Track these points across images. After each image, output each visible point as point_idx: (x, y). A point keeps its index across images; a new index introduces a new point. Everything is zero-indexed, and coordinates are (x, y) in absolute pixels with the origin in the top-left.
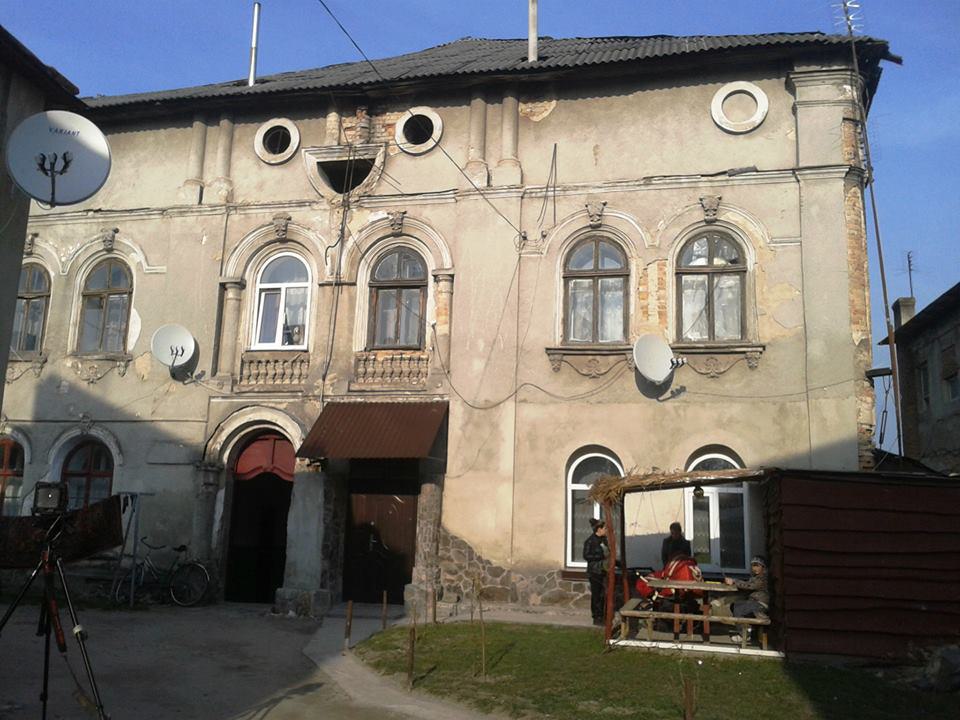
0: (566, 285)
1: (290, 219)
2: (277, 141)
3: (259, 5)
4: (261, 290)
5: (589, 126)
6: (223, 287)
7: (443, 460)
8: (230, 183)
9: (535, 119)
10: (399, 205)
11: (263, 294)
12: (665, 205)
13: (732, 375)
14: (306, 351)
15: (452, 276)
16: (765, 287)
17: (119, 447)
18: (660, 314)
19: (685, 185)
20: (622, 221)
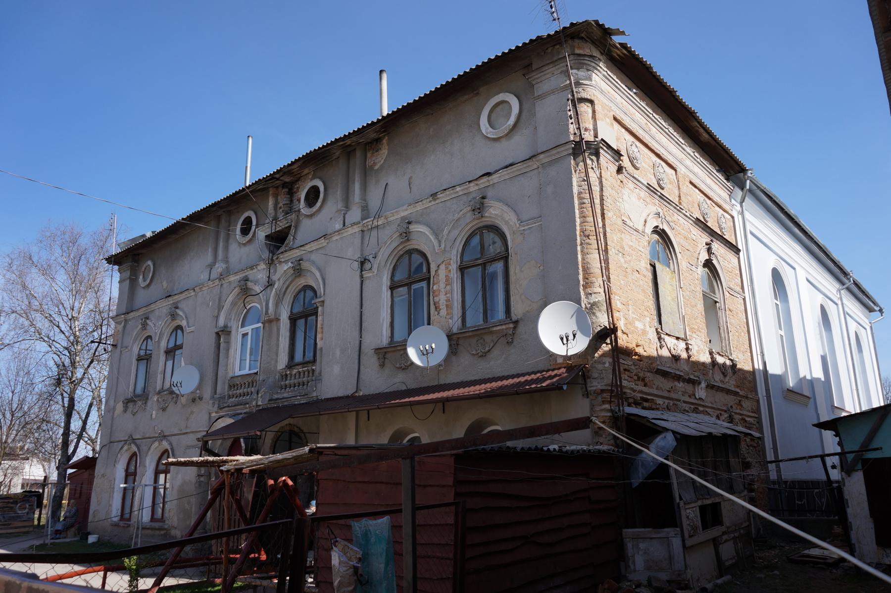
6: (217, 333)
13: (496, 352)
14: (256, 373)
18: (447, 306)
19: (461, 193)
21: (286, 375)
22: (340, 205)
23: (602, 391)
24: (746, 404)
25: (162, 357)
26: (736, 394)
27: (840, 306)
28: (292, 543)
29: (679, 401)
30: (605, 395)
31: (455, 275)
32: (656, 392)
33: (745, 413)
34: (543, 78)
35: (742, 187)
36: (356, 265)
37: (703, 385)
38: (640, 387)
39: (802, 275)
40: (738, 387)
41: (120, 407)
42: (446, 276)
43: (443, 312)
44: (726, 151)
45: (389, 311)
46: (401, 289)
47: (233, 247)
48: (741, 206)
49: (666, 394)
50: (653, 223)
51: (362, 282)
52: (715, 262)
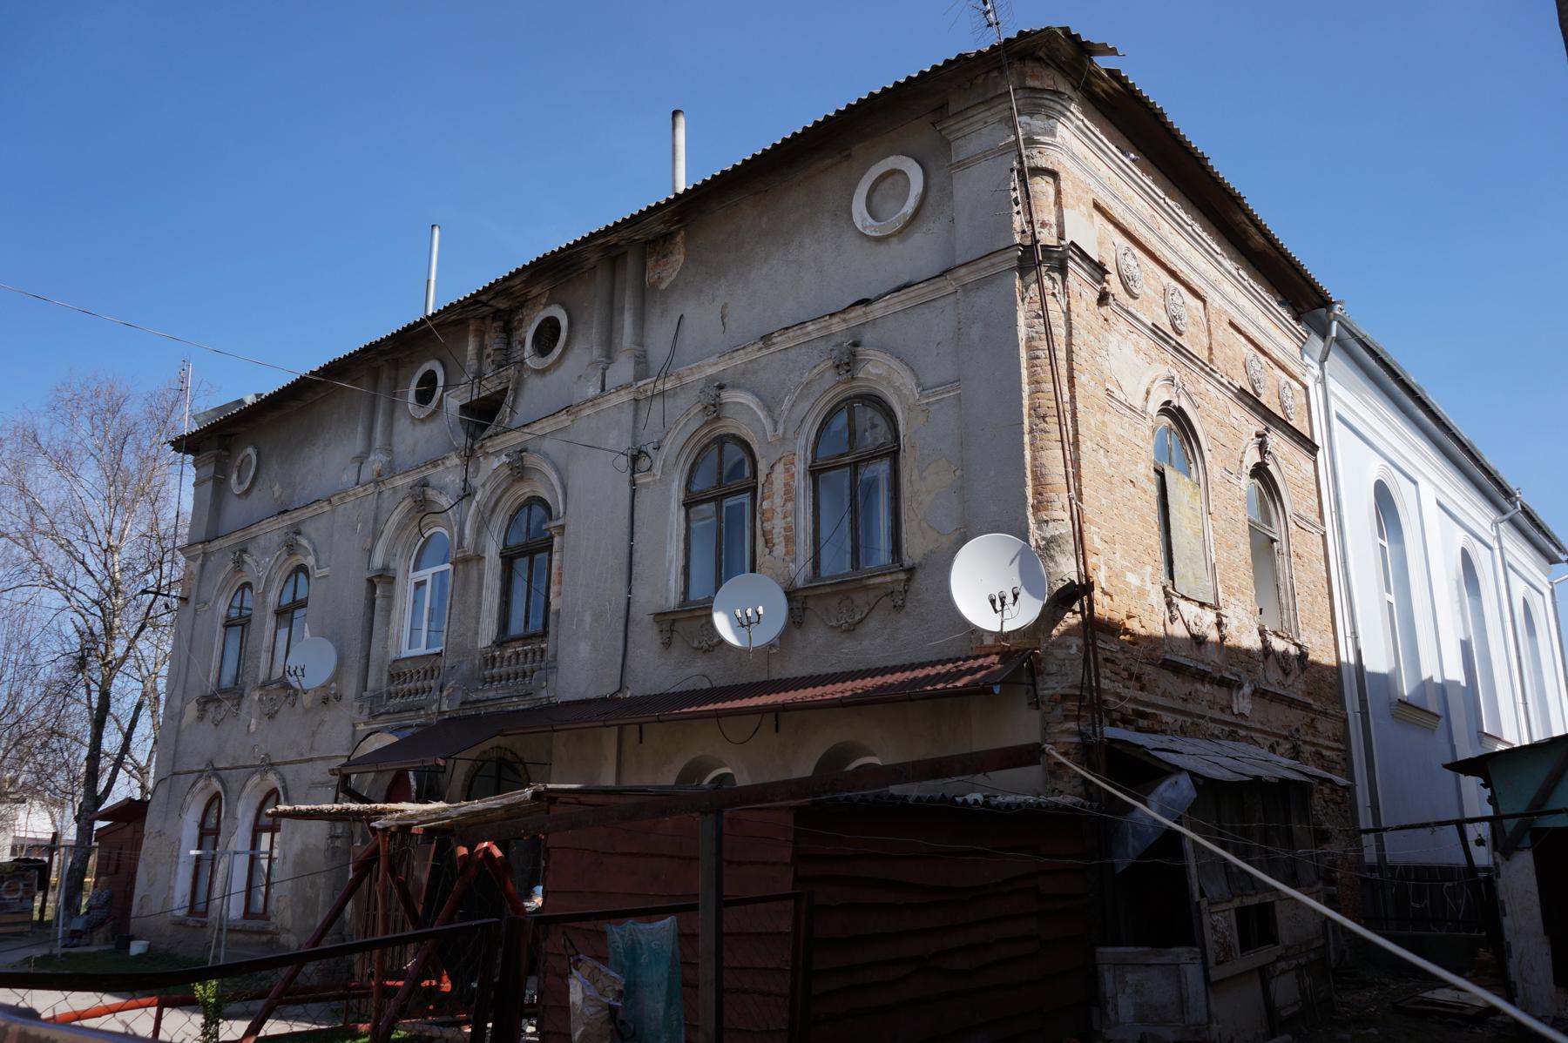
2: (425, 394)
6: (370, 581)
9: (663, 286)
13: (873, 624)
14: (439, 654)
16: (916, 472)
19: (814, 336)
20: (746, 413)
21: (494, 658)
22: (596, 353)
23: (1065, 697)
24: (1324, 725)
25: (270, 622)
26: (1306, 707)
27: (1497, 552)
28: (499, 962)
29: (1203, 717)
30: (1069, 704)
31: (801, 482)
32: (1161, 701)
33: (1321, 741)
34: (967, 130)
35: (1324, 334)
36: (624, 462)
37: (1247, 689)
38: (1133, 692)
39: (1428, 495)
40: (1309, 694)
41: (192, 711)
42: (787, 485)
43: (780, 549)
44: (1296, 268)
45: (682, 546)
46: (704, 506)
47: (402, 425)
48: (1322, 368)
49: (1179, 705)
50: (1161, 395)
51: (634, 493)
52: (1272, 468)
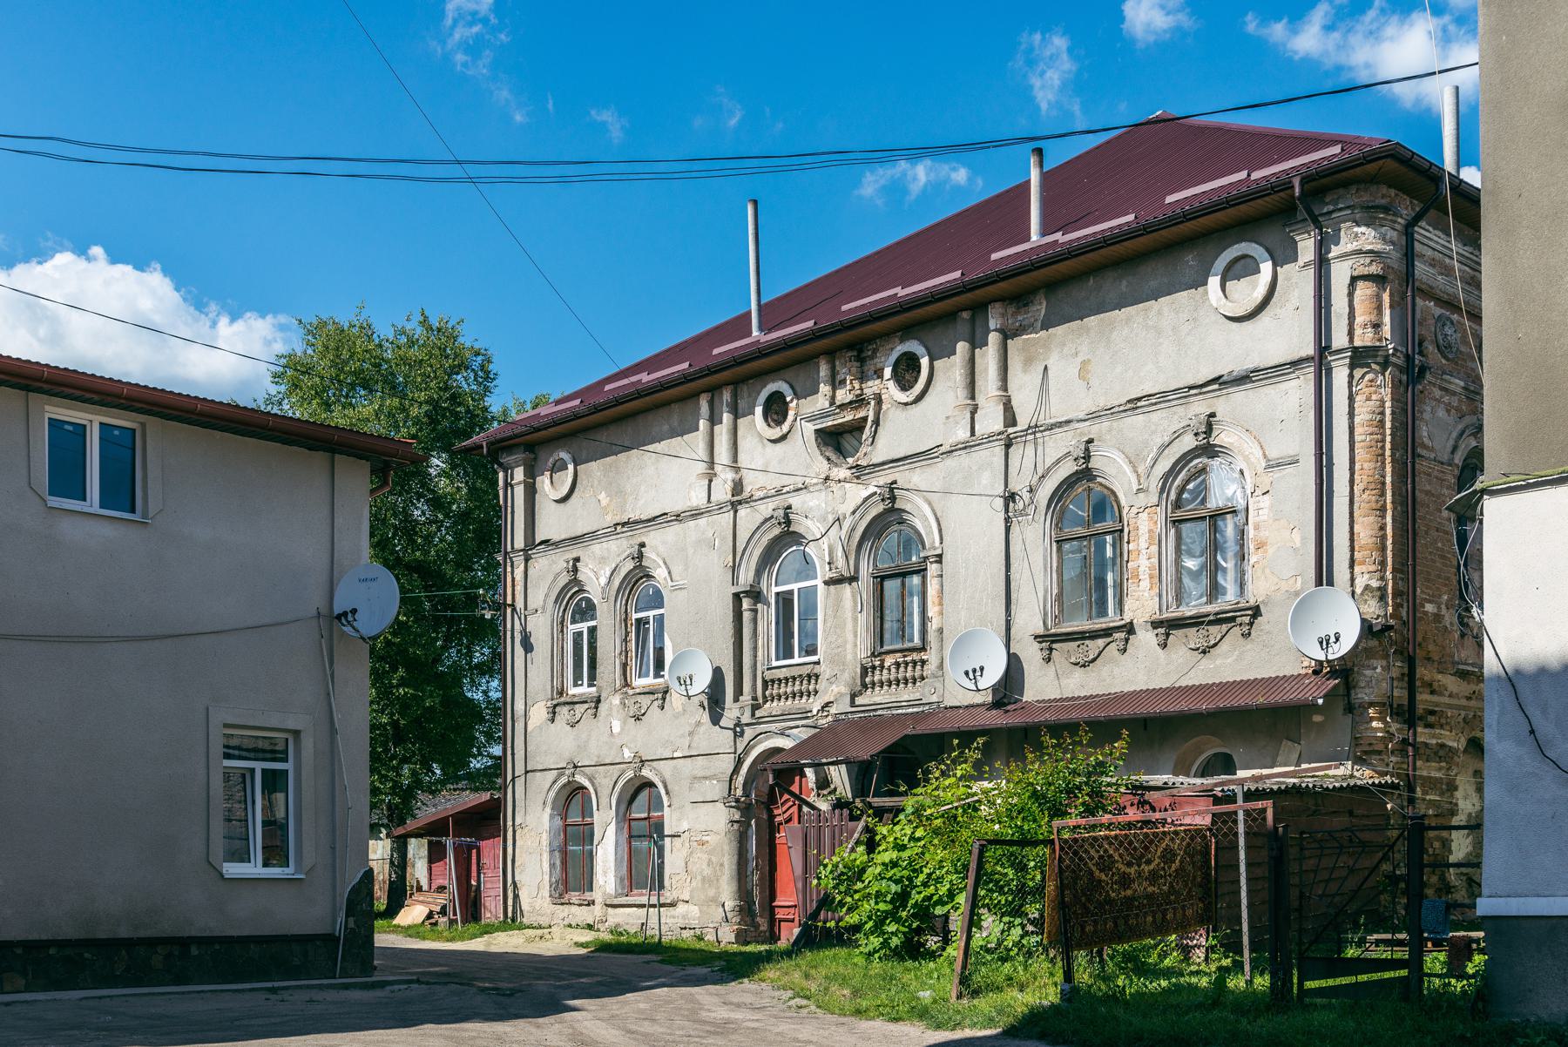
0: (1059, 549)
1: (789, 507)
3: (755, 202)
4: (923, 649)
5: (1080, 335)
6: (737, 597)
7: (584, 457)
8: (737, 470)
10: (884, 478)
11: (917, 640)
12: (1154, 432)
13: (1224, 646)
15: (940, 556)
17: (666, 787)
